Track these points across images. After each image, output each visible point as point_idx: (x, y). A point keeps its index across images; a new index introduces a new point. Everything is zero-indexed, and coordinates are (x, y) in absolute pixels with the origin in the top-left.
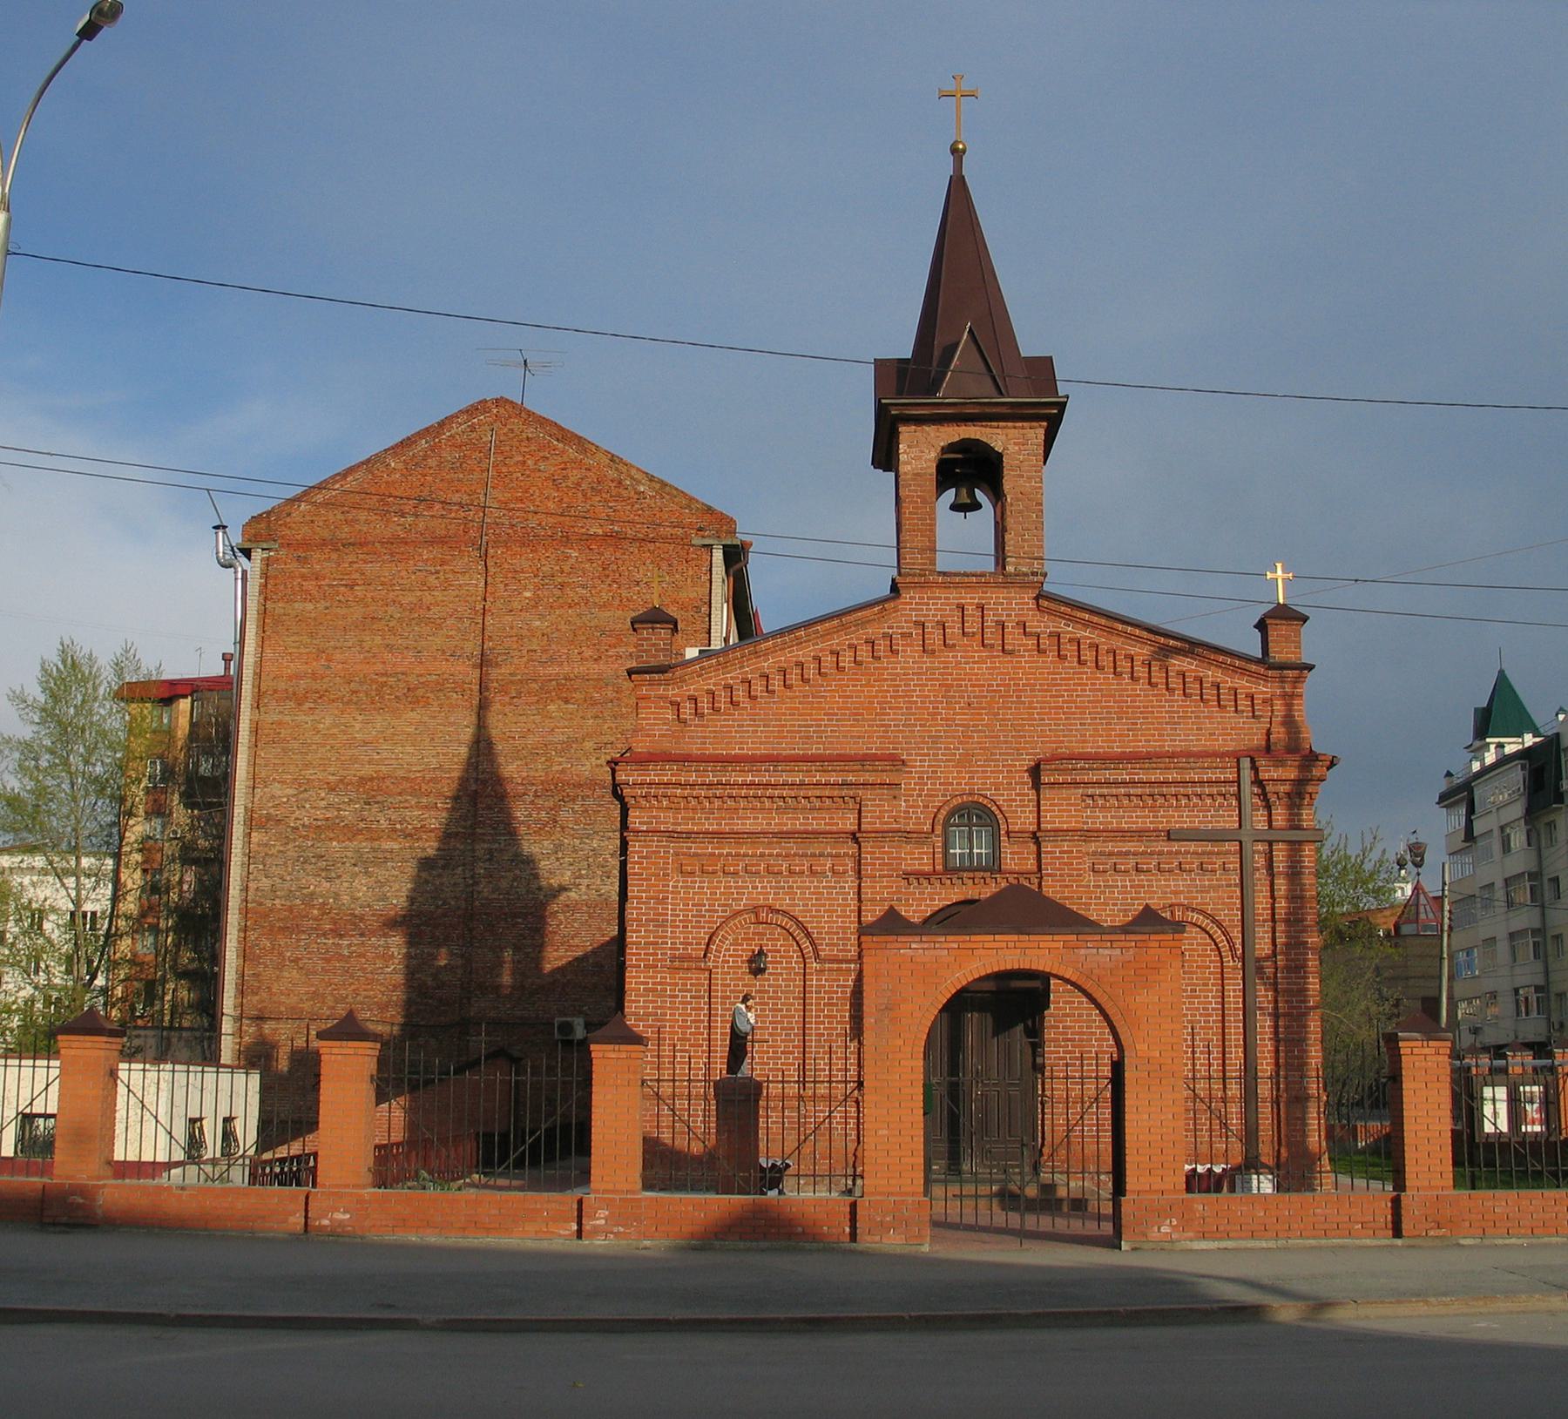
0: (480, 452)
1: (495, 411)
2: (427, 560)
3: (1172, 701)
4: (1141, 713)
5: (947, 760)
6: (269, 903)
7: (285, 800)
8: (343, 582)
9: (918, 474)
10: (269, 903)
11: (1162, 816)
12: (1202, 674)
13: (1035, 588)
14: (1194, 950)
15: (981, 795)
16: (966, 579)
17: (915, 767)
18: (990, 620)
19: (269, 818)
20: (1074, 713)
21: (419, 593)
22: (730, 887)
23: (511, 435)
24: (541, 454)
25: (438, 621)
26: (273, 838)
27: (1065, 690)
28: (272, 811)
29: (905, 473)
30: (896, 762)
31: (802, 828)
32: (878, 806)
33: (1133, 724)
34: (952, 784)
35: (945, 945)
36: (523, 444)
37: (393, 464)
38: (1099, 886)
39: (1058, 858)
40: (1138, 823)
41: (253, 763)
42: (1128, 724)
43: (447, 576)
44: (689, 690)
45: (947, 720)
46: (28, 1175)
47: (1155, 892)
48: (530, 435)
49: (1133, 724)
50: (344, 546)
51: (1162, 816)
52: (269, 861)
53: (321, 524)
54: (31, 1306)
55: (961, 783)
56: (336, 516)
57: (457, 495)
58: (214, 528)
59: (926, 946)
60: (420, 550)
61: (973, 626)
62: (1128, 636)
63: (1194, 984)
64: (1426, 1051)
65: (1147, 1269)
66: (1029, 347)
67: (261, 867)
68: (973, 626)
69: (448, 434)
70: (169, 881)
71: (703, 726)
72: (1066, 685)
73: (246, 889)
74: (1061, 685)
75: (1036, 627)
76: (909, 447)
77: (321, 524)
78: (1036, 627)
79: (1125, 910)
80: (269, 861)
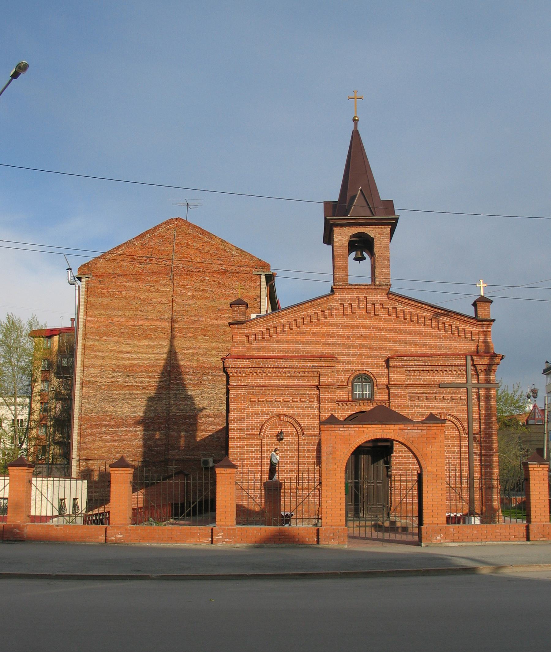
0: (170, 239)
1: (176, 223)
2: (150, 281)
6: (90, 415)
7: (96, 375)
8: (118, 290)
9: (341, 246)
10: (90, 415)
11: (436, 379)
12: (452, 323)
13: (387, 290)
16: (360, 287)
18: (369, 302)
19: (89, 382)
21: (147, 294)
22: (269, 407)
23: (182, 232)
24: (194, 240)
25: (155, 305)
26: (92, 390)
28: (91, 379)
30: (333, 358)
31: (297, 384)
36: (187, 236)
37: (136, 244)
38: (412, 406)
40: (427, 381)
41: (83, 361)
42: (423, 343)
43: (158, 287)
48: (190, 232)
49: (425, 343)
50: (118, 276)
52: (90, 398)
55: (358, 366)
56: (114, 264)
57: (162, 256)
60: (147, 277)
61: (363, 305)
62: (423, 309)
66: (384, 197)
67: (87, 401)
68: (363, 305)
69: (158, 232)
71: (258, 345)
72: (399, 328)
73: (81, 410)
74: (397, 328)
75: (387, 305)
76: (337, 236)
78: (387, 305)
80: (90, 398)
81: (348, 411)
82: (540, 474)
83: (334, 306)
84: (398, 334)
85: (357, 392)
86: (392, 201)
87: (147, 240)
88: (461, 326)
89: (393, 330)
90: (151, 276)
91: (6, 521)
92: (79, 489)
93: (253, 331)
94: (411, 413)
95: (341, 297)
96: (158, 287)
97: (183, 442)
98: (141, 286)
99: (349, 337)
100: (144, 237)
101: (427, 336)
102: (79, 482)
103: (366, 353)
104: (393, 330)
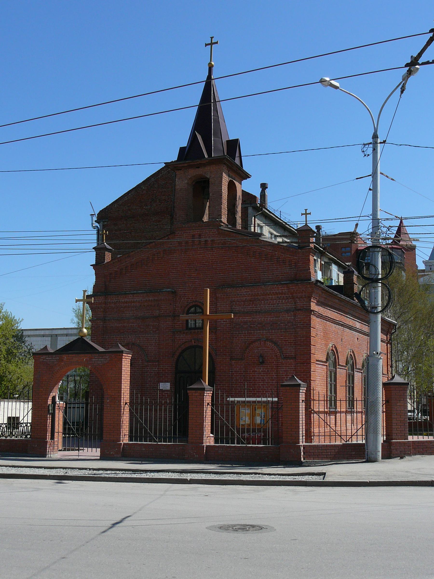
2: (154, 221)
3: (264, 264)
4: (262, 268)
5: (190, 290)
11: (259, 307)
14: (268, 356)
15: (199, 302)
17: (178, 293)
20: (230, 271)
21: (152, 233)
22: (121, 337)
27: (228, 263)
29: (178, 189)
32: (165, 307)
33: (250, 273)
34: (190, 298)
35: (55, 358)
37: (143, 188)
38: (236, 333)
39: (222, 324)
43: (161, 226)
44: (110, 271)
45: (189, 276)
46: (400, 441)
47: (255, 335)
49: (250, 273)
51: (259, 307)
53: (121, 211)
54: (267, 486)
58: (91, 215)
59: (50, 358)
60: (152, 218)
63: (269, 369)
64: (196, 394)
65: (185, 469)
69: (161, 175)
70: (9, 338)
74: (226, 261)
77: (121, 211)
79: (245, 342)
81: (183, 340)
82: (198, 399)
83: (174, 244)
84: (227, 267)
85: (193, 322)
86: (180, 147)
87: (152, 183)
88: (282, 256)
89: (223, 263)
90: (155, 216)
91: (408, 440)
92: (18, 409)
93: (110, 271)
94: (235, 340)
95: (180, 235)
96: (161, 226)
97: (86, 369)
98: (147, 226)
99: (186, 272)
100: (150, 181)
101: (252, 267)
102: (344, 402)
103: (200, 285)
104: (223, 263)
